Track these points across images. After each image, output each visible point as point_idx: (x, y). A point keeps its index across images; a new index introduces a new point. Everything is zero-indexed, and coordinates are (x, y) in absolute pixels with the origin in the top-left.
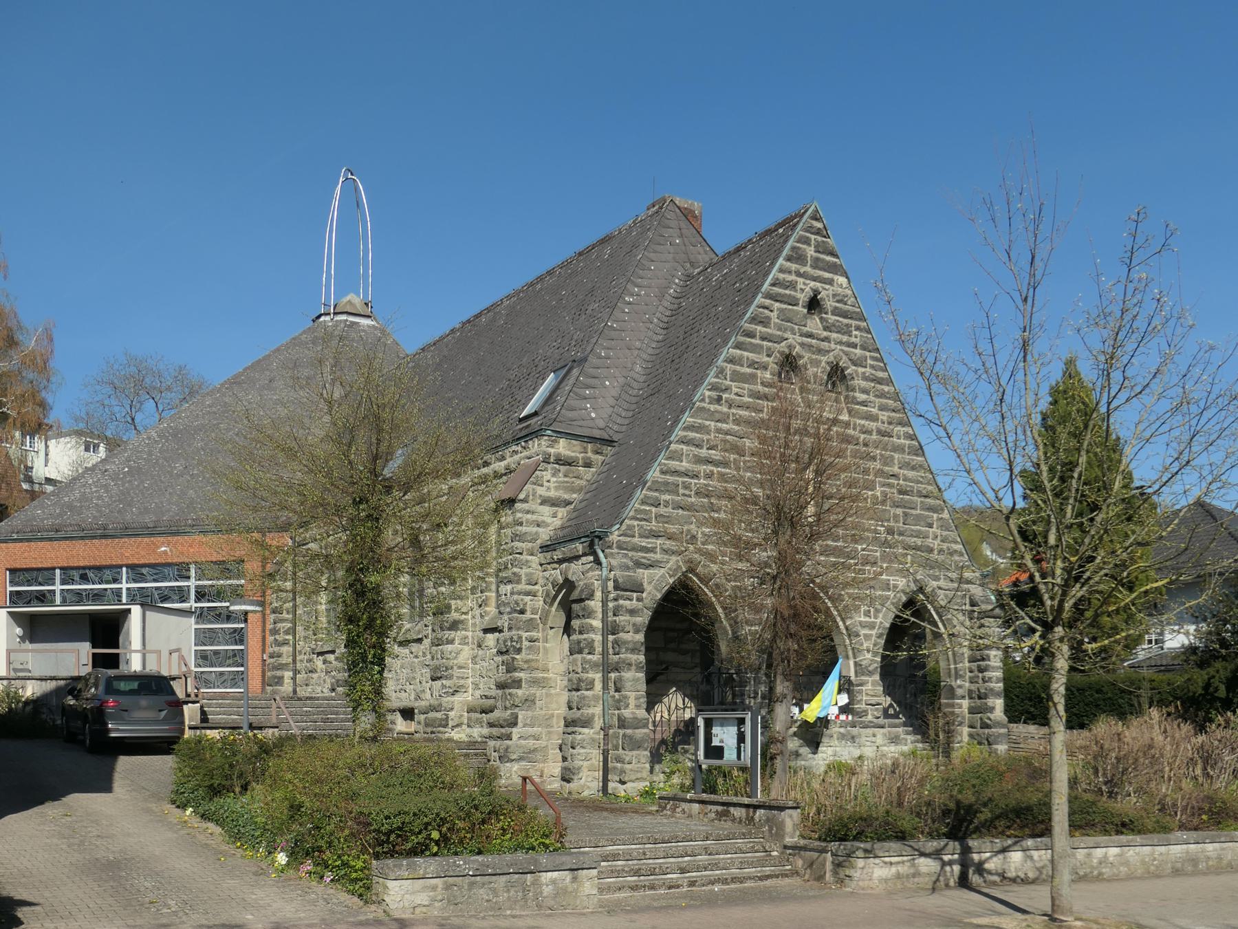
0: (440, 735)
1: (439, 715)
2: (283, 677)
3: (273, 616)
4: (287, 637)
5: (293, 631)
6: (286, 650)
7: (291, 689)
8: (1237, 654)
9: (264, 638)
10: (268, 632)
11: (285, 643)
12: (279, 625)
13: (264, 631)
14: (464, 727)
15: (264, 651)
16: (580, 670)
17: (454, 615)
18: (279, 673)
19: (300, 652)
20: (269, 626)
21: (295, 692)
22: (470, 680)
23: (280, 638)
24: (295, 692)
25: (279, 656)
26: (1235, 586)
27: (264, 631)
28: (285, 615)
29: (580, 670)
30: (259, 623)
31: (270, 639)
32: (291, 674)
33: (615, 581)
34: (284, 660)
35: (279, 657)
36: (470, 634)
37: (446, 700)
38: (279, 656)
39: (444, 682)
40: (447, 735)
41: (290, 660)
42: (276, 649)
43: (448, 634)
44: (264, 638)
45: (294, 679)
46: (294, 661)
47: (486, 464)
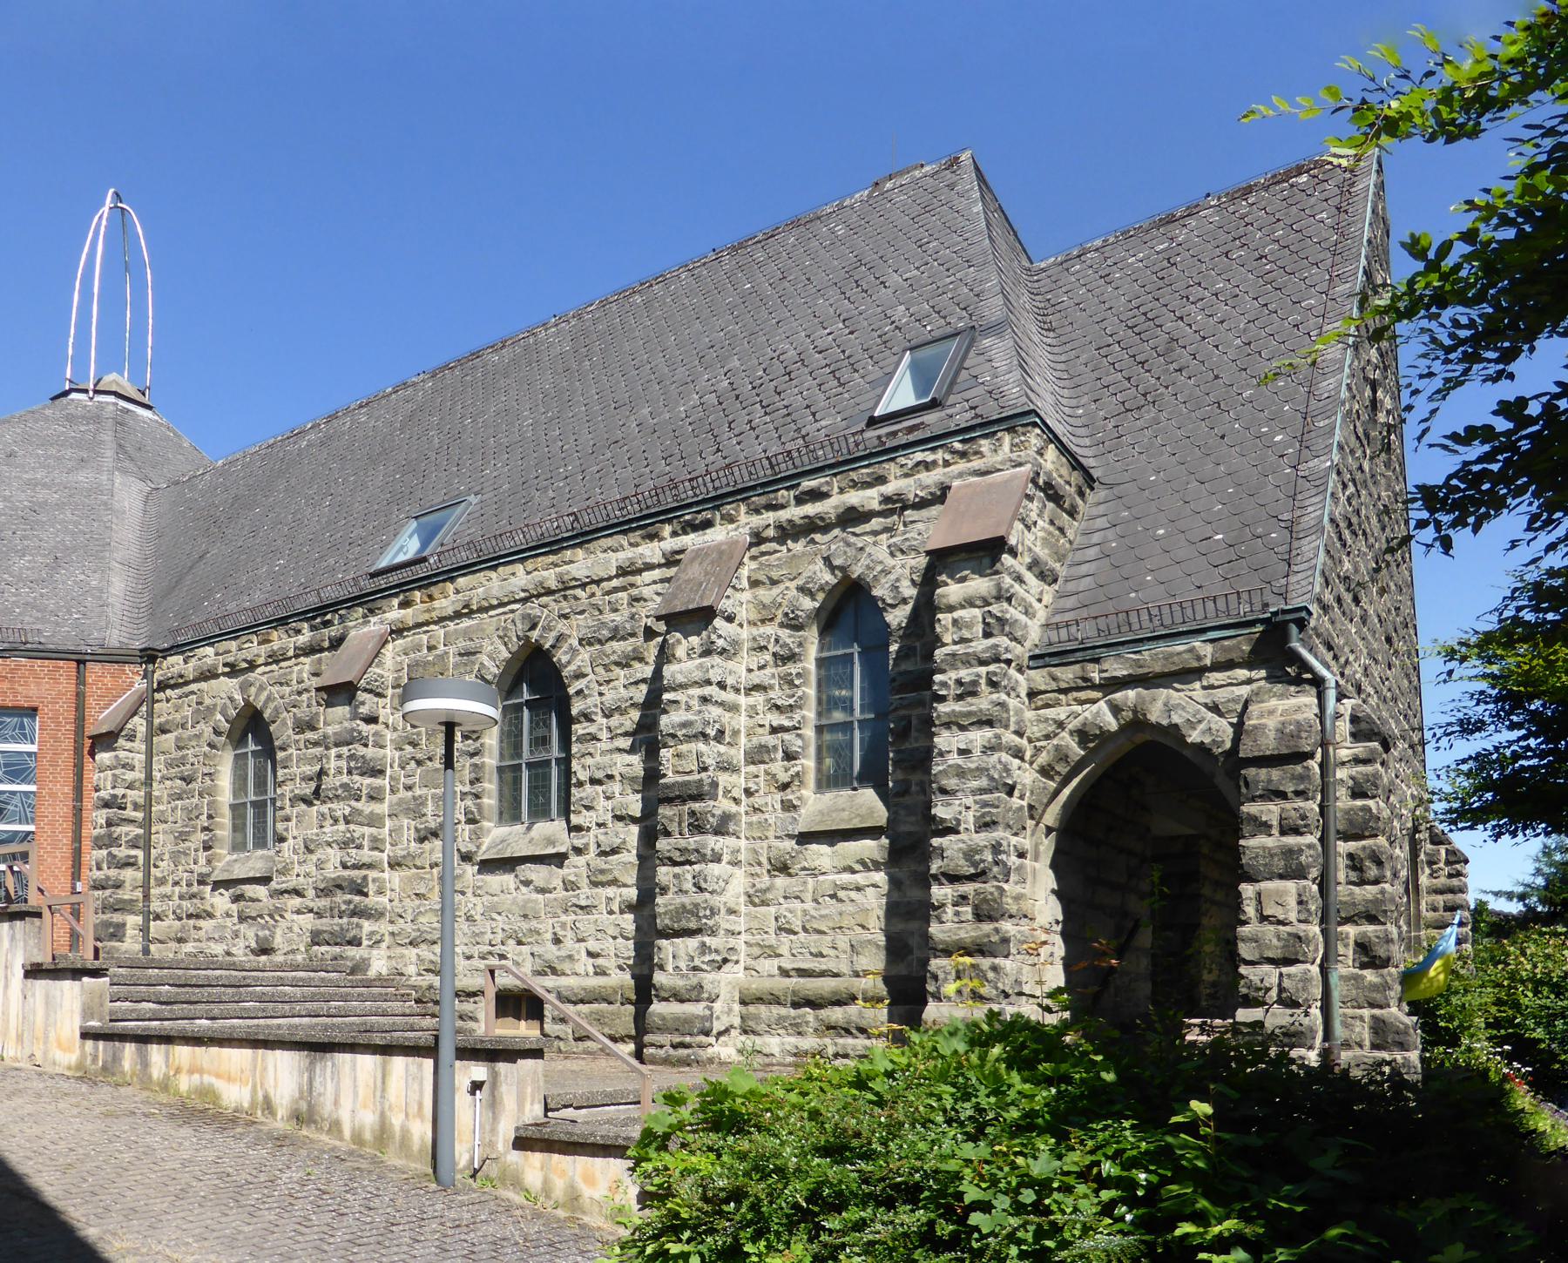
0: (700, 1051)
1: (697, 1009)
2: (124, 925)
3: (101, 816)
4: (133, 852)
5: (144, 843)
6: (129, 874)
7: (138, 947)
8: (1565, 661)
9: (77, 855)
10: (86, 844)
11: (129, 863)
12: (118, 830)
13: (77, 838)
14: (734, 1033)
15: (76, 875)
16: (1293, 916)
17: (723, 805)
18: (117, 918)
19: (162, 882)
20: (90, 832)
21: (146, 951)
22: (743, 937)
23: (122, 852)
24: (146, 951)
25: (118, 885)
26: (1557, 990)
27: (77, 838)
28: (130, 813)
29: (1293, 916)
30: (68, 826)
31: (93, 855)
32: (139, 919)
33: (1355, 719)
34: (125, 894)
35: (118, 887)
36: (743, 843)
37: (708, 978)
38: (118, 885)
39: (707, 939)
40: (710, 1050)
41: (139, 894)
42: (113, 873)
43: (712, 842)
44: (77, 855)
45: (145, 930)
46: (147, 897)
47: (817, 495)
